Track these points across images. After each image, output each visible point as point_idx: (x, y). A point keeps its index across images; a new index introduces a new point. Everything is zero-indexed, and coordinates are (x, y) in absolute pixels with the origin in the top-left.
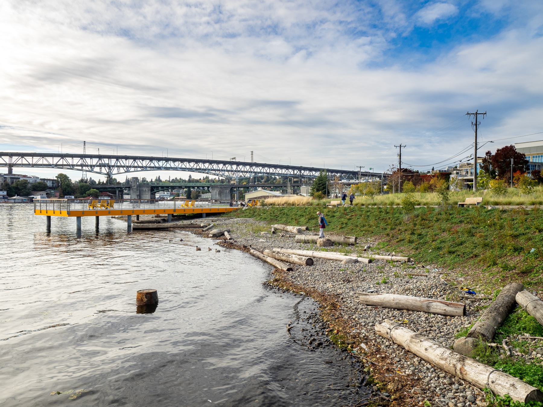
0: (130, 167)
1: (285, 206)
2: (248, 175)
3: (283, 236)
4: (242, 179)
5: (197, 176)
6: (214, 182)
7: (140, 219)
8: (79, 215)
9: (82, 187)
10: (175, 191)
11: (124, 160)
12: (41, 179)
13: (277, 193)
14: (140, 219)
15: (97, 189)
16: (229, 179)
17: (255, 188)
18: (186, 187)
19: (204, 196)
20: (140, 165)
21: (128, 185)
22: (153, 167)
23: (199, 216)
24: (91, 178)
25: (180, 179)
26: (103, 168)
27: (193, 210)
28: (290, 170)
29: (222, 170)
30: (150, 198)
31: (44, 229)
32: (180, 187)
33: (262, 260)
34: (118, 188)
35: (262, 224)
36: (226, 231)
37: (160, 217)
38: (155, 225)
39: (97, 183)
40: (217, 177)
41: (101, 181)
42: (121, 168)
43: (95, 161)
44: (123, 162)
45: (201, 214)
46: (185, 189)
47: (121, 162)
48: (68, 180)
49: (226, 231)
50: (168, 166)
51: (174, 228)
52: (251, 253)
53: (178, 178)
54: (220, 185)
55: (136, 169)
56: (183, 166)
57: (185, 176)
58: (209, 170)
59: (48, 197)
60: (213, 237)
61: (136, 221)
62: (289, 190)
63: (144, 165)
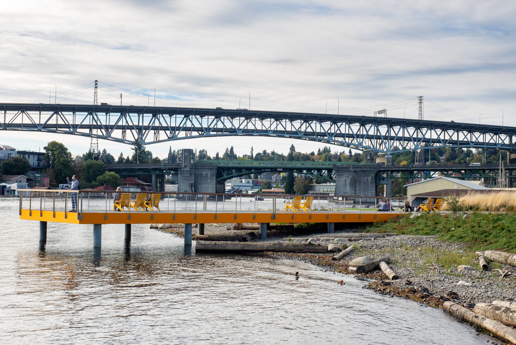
0: (178, 129)
1: (502, 211)
2: (411, 146)
3: (506, 276)
4: (398, 155)
5: (306, 147)
6: (340, 160)
7: (207, 233)
8: (97, 221)
9: (89, 167)
10: (261, 178)
11: (166, 116)
12: (19, 152)
13: (477, 184)
14: (207, 233)
15: (117, 171)
16: (372, 154)
17: (426, 173)
18: (285, 170)
19: (321, 188)
20: (197, 125)
21: (175, 165)
22: (221, 130)
23: (320, 228)
24: (105, 151)
25: (273, 153)
26: (128, 131)
27: (310, 216)
28: (503, 136)
29: (358, 136)
30: (214, 191)
31: (36, 244)
32: (274, 170)
33: (471, 324)
34: (155, 170)
35: (455, 250)
36: (383, 260)
37: (243, 228)
38: (238, 245)
39: (116, 159)
40: (346, 150)
41: (125, 157)
42: (162, 132)
43: (113, 118)
44: (165, 120)
45: (325, 224)
46: (282, 174)
47: (161, 119)
48: (67, 154)
49: (383, 260)
50: (251, 127)
51: (275, 251)
52: (445, 310)
53: (269, 151)
54: (354, 167)
55: (189, 133)
56: (280, 128)
57: (281, 147)
58: (331, 135)
59: (30, 186)
60: (358, 272)
61: (198, 235)
62: (502, 179)
63: (205, 126)
